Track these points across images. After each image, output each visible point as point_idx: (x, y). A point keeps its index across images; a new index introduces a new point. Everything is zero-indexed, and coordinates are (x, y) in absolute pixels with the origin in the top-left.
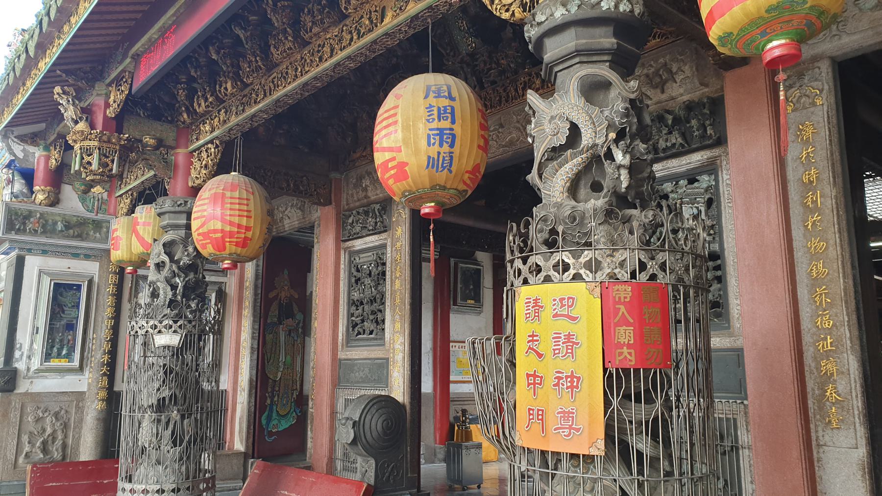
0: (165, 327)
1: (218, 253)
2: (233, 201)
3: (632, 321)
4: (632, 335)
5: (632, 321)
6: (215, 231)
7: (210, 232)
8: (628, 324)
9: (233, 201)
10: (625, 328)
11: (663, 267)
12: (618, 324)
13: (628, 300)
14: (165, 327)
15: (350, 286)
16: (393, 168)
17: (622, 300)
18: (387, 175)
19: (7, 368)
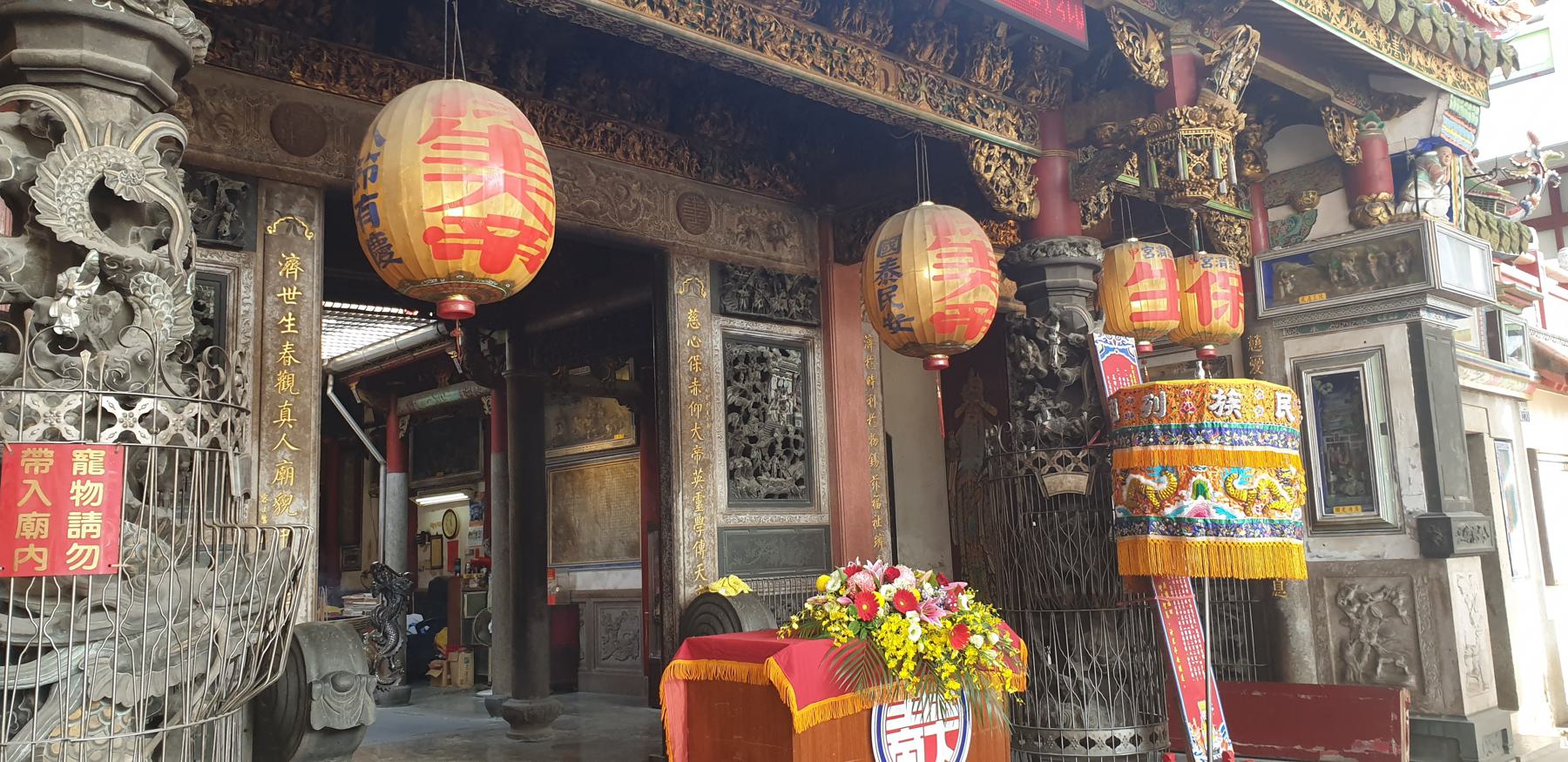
0: (1060, 461)
1: (483, 274)
2: (456, 169)
3: (48, 504)
4: (46, 526)
5: (48, 504)
6: (505, 222)
7: (490, 220)
8: (42, 508)
9: (456, 169)
10: (35, 514)
11: (1022, 465)
12: (28, 509)
13: (46, 471)
14: (1060, 461)
15: (806, 432)
16: (537, 248)
17: (36, 470)
18: (522, 247)
19: (1435, 515)
